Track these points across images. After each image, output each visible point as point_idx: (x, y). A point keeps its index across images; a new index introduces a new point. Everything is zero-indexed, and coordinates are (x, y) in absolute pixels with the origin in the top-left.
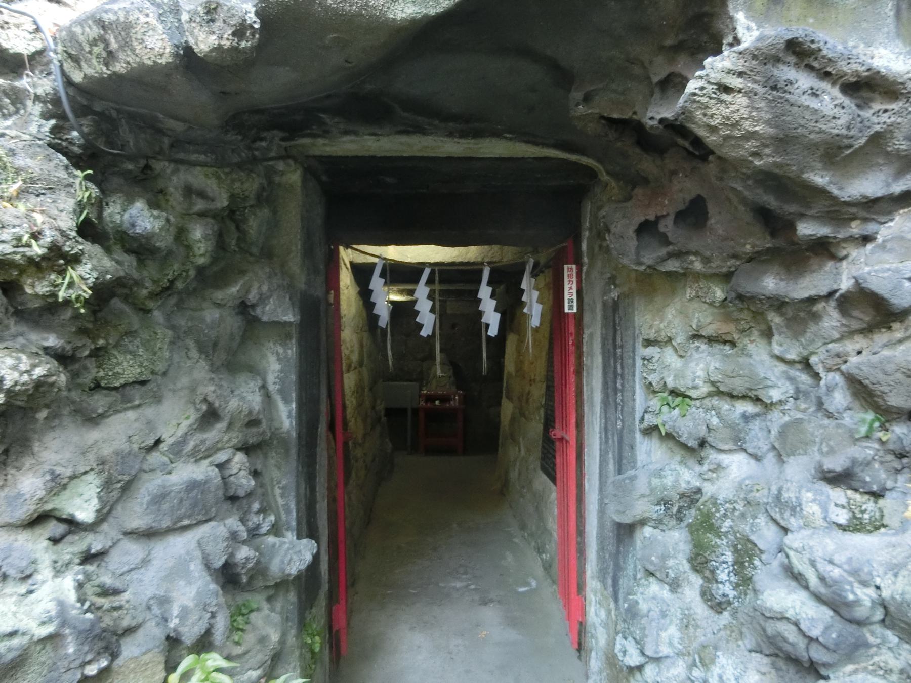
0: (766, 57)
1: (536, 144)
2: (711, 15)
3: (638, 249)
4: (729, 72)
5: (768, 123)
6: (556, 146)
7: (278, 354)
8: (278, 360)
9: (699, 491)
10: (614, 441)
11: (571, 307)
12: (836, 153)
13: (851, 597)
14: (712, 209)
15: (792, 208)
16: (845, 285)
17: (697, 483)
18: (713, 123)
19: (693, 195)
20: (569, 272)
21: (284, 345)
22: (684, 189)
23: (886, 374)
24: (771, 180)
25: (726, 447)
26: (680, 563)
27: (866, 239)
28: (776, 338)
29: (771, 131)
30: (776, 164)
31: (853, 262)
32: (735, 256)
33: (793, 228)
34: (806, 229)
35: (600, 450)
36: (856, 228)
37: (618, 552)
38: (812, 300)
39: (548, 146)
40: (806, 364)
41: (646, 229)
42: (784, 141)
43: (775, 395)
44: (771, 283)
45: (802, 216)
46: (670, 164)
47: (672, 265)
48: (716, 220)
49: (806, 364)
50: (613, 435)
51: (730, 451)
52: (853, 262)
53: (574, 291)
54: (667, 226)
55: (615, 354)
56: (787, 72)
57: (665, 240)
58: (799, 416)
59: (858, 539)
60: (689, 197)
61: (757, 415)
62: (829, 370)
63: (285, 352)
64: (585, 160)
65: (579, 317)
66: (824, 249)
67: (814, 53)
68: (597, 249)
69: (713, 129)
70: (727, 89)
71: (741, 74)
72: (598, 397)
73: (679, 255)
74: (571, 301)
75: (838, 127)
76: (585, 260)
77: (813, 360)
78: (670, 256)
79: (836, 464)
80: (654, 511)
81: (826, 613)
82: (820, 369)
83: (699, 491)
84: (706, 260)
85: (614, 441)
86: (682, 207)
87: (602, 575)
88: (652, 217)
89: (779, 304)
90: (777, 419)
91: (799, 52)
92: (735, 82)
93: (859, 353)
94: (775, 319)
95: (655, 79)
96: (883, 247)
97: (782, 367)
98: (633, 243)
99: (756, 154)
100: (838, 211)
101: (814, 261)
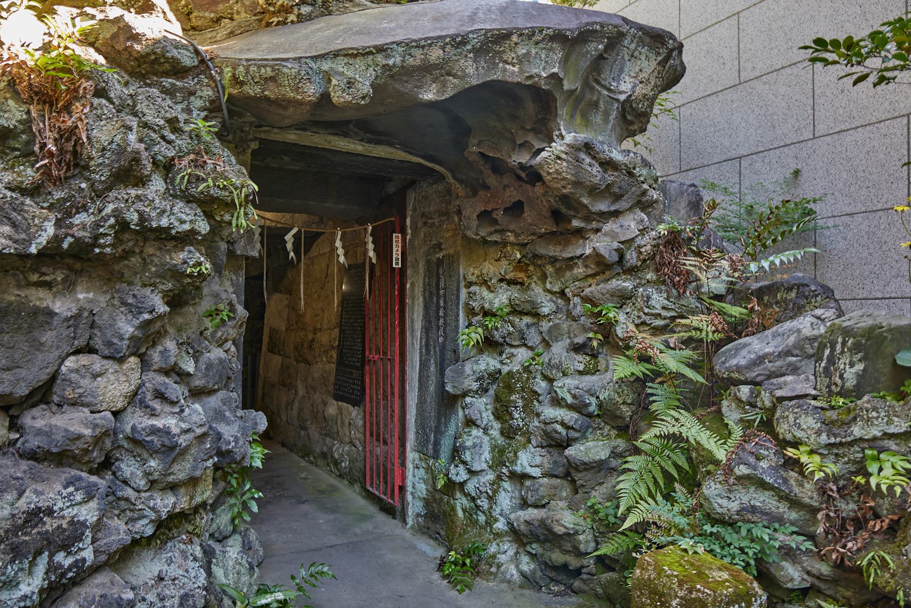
0: (575, 148)
1: (410, 153)
2: (549, 120)
3: (478, 226)
4: (562, 152)
5: (572, 175)
6: (423, 157)
7: (231, 280)
8: (232, 284)
9: (500, 371)
10: (435, 352)
11: (397, 263)
12: (594, 191)
13: (588, 401)
14: (526, 208)
15: (572, 213)
16: (588, 251)
17: (498, 366)
18: (551, 171)
19: (516, 199)
20: (397, 238)
21: (236, 274)
22: (512, 195)
23: (602, 294)
24: (565, 199)
25: (516, 343)
26: (487, 416)
27: (598, 230)
28: (549, 279)
29: (573, 178)
30: (571, 193)
31: (592, 240)
32: (533, 234)
33: (570, 222)
34: (576, 223)
35: (420, 361)
36: (594, 225)
37: (439, 423)
38: (572, 258)
39: (418, 156)
40: (562, 294)
41: (485, 216)
42: (577, 184)
43: (545, 311)
44: (553, 251)
45: (575, 216)
46: (506, 181)
47: (496, 238)
48: (529, 215)
49: (562, 294)
50: (435, 348)
51: (518, 346)
52: (592, 240)
53: (400, 252)
54: (499, 215)
55: (438, 293)
56: (582, 156)
57: (495, 222)
58: (558, 321)
59: (588, 378)
60: (513, 200)
61: (534, 324)
62: (574, 296)
63: (237, 279)
64: (437, 167)
65: (403, 271)
66: (580, 233)
67: (592, 149)
68: (420, 224)
69: (549, 173)
70: (559, 158)
71: (566, 154)
72: (418, 325)
73: (501, 232)
74: (397, 259)
75: (596, 180)
76: (409, 231)
77: (567, 290)
78: (496, 231)
79: (580, 340)
80: (475, 386)
81: (575, 415)
82: (570, 295)
83: (500, 371)
84: (517, 235)
85: (435, 352)
86: (508, 205)
87: (421, 448)
88: (490, 209)
89: (554, 260)
90: (545, 325)
91: (588, 147)
92: (564, 156)
93: (590, 286)
94: (550, 269)
95: (518, 143)
96: (605, 235)
97: (550, 296)
98: (475, 223)
99: (564, 187)
100: (589, 216)
101: (573, 240)
